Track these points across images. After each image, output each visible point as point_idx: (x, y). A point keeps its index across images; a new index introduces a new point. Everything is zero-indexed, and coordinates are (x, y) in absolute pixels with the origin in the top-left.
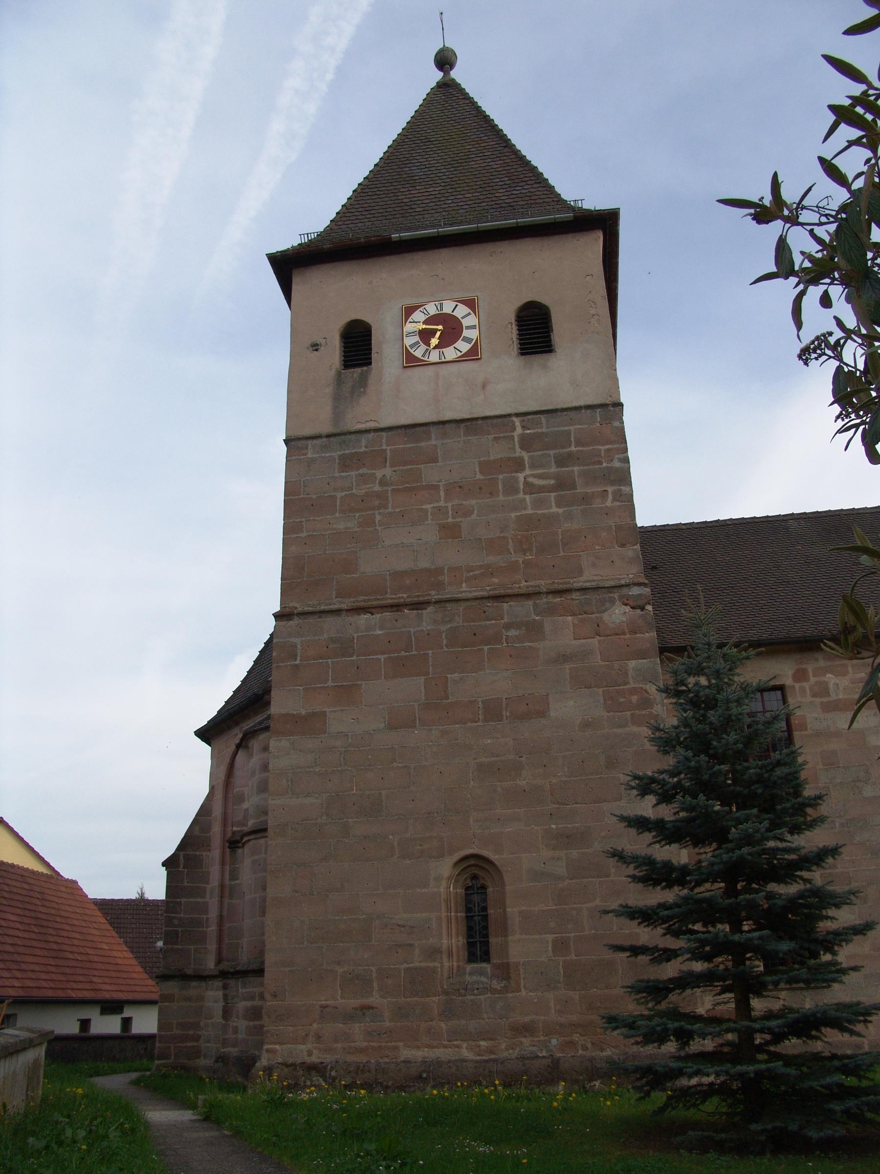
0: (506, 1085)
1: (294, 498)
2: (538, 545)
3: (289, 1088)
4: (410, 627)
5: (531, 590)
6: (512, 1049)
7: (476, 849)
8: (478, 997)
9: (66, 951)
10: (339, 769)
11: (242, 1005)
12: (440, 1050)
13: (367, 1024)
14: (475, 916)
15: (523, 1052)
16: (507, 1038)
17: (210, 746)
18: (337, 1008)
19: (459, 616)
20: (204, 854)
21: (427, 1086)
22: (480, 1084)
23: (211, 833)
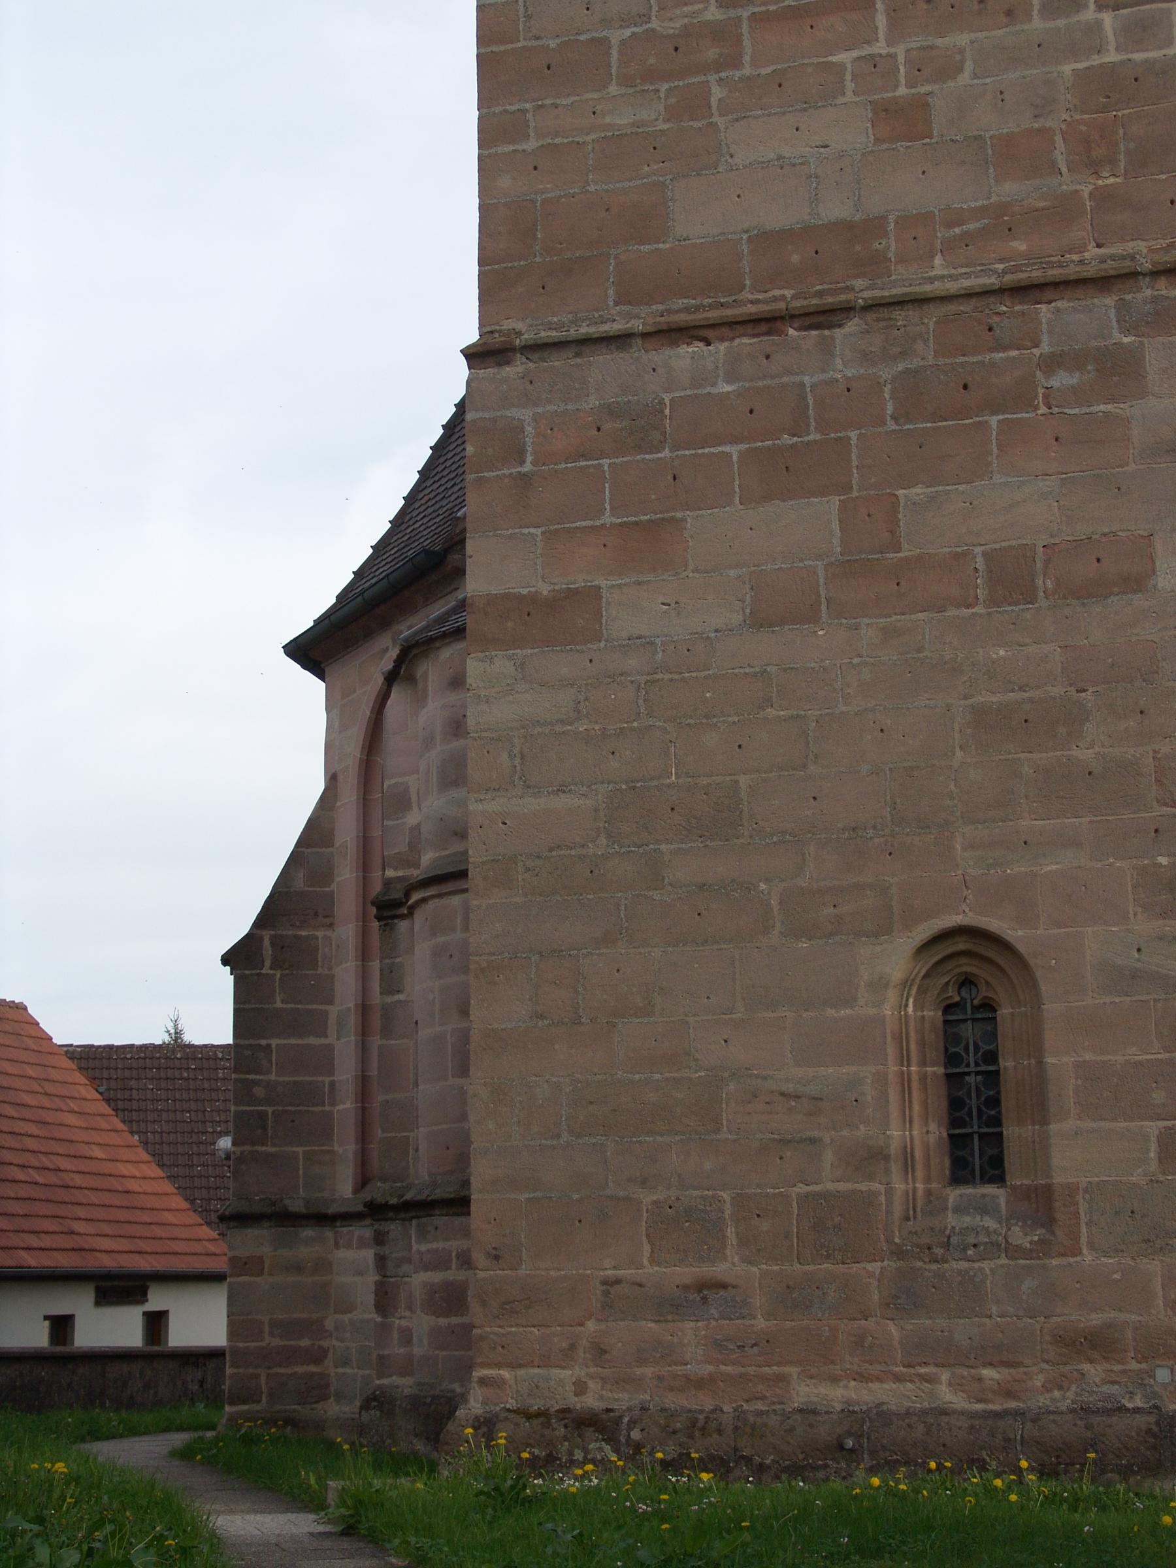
0: (1045, 1472)
1: (502, 48)
2: (1132, 145)
3: (534, 1465)
4: (803, 373)
5: (1111, 267)
6: (1060, 1388)
7: (970, 914)
8: (976, 1265)
9: (11, 1164)
10: (635, 724)
11: (419, 1281)
12: (886, 1386)
13: (714, 1323)
14: (968, 1074)
15: (1087, 1398)
16: (1047, 1362)
17: (322, 678)
18: (641, 1285)
19: (926, 341)
20: (320, 934)
21: (857, 1468)
22: (983, 1467)
23: (334, 886)
